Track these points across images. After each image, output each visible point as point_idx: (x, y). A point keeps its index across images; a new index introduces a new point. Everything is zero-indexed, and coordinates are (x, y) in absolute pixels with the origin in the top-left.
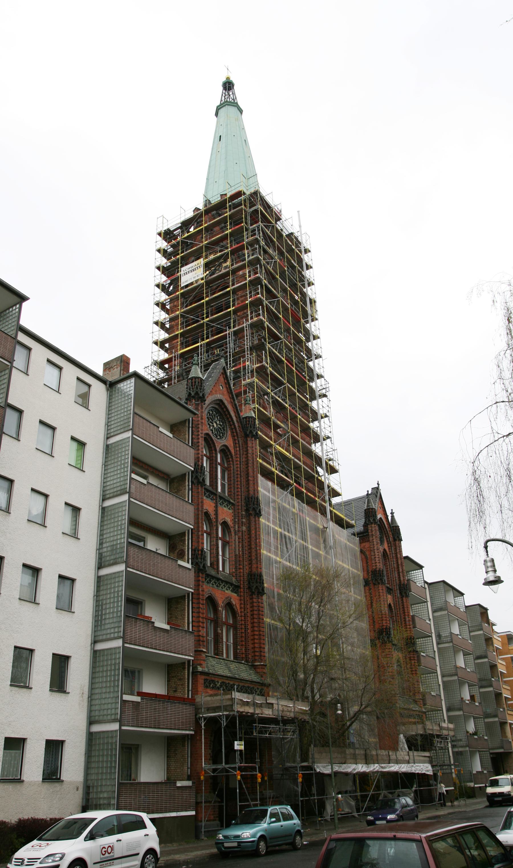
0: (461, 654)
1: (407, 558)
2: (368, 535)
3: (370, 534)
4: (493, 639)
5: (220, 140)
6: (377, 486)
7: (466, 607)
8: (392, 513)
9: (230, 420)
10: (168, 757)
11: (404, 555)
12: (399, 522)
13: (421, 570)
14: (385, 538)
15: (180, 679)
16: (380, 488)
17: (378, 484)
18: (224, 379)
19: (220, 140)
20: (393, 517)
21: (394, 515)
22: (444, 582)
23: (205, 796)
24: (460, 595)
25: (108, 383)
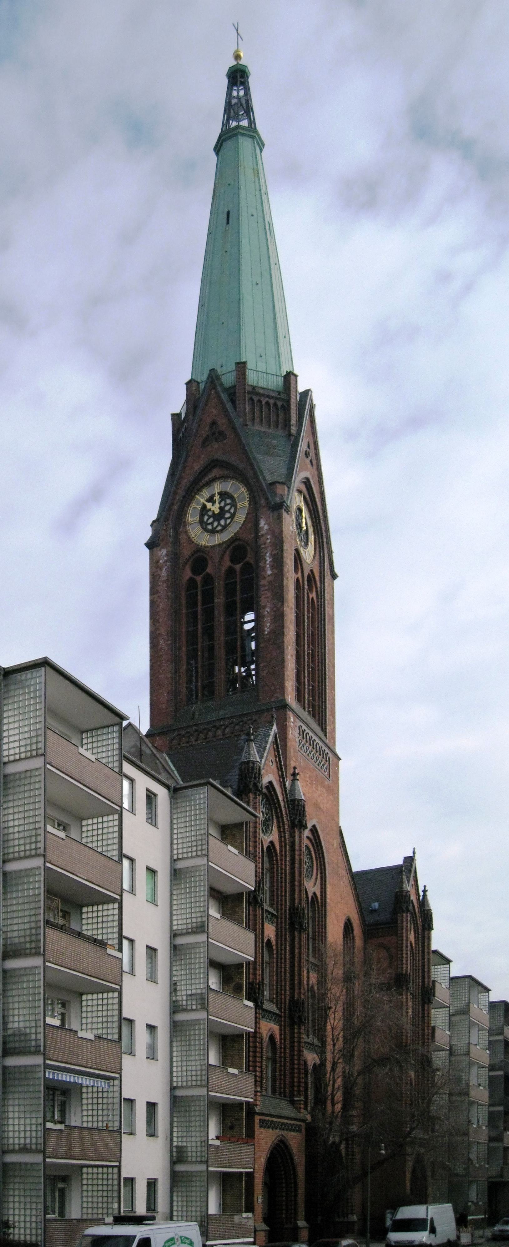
0: (476, 1067)
1: (435, 952)
2: (397, 927)
3: (399, 925)
4: (219, 838)
5: (228, 223)
6: (412, 855)
7: (452, 979)
8: (425, 891)
9: (277, 806)
10: (223, 1190)
11: (433, 948)
12: (435, 905)
13: (448, 966)
14: (275, 821)
15: (237, 1119)
16: (416, 858)
17: (414, 852)
18: (275, 750)
19: (228, 223)
20: (425, 895)
21: (427, 893)
22: (470, 977)
23: (328, 1237)
24: (443, 962)
25: (172, 789)
